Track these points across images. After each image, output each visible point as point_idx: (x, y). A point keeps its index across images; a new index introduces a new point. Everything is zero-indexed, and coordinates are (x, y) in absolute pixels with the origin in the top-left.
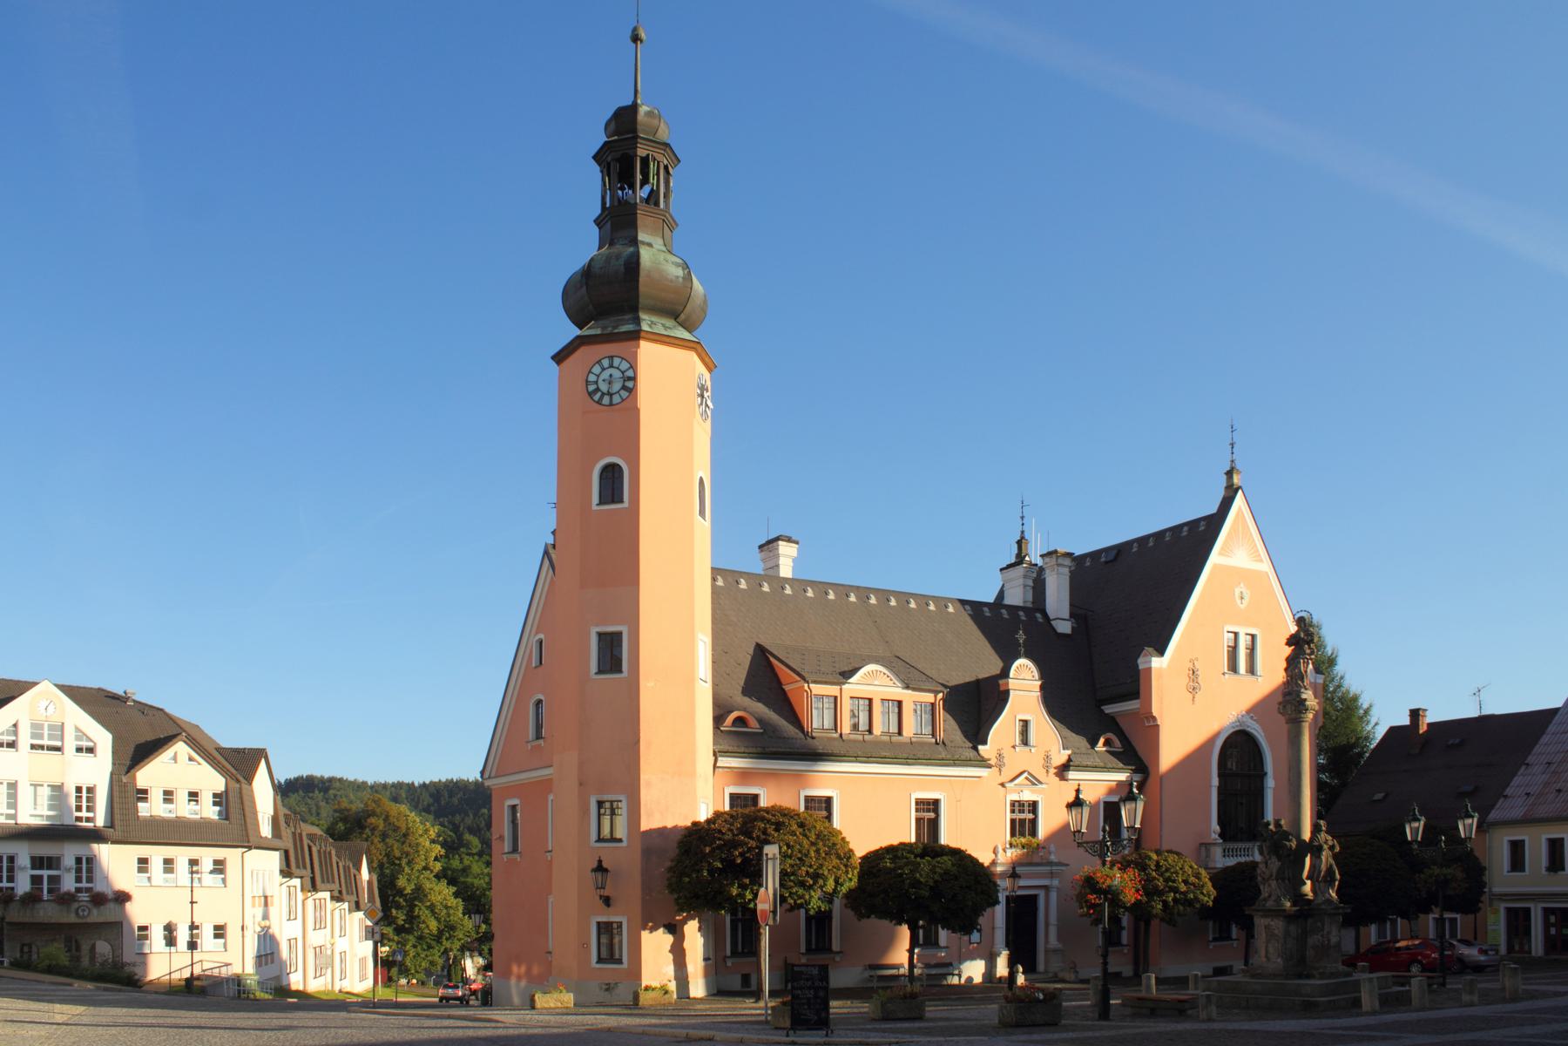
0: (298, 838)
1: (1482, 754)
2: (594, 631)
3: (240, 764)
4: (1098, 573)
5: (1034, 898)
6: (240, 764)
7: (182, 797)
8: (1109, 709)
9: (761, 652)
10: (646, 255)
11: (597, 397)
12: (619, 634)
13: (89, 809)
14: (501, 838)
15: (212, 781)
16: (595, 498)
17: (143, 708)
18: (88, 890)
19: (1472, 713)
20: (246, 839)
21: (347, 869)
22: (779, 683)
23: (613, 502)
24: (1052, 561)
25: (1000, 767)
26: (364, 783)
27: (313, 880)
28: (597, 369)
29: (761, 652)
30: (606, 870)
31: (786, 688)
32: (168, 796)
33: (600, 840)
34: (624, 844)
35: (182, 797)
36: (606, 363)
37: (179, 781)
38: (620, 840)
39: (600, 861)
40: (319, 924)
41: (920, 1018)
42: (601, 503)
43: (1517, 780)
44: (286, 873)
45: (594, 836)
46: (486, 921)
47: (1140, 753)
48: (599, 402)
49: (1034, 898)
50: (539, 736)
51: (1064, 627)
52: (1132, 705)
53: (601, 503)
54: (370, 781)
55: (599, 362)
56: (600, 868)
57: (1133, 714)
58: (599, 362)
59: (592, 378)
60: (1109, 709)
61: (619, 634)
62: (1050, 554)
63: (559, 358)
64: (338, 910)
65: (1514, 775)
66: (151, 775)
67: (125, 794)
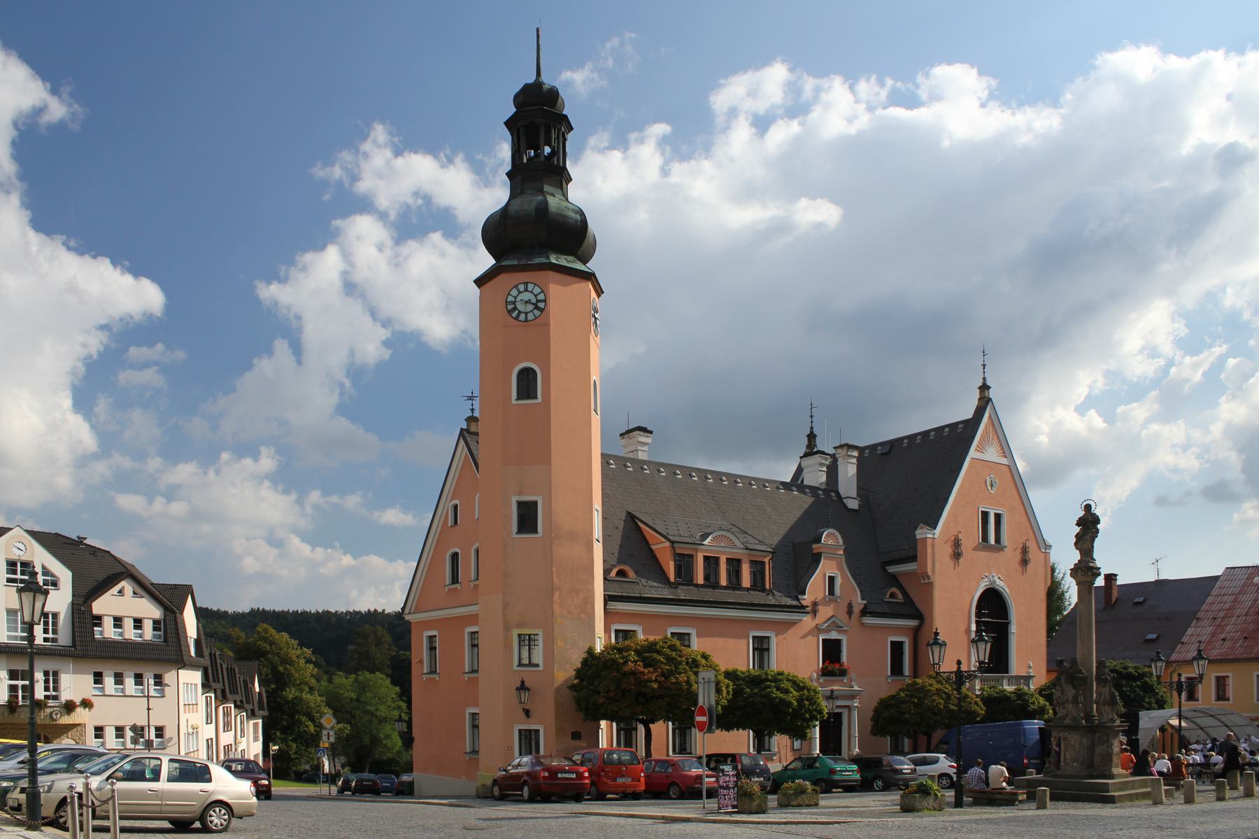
0: (213, 657)
1: (1164, 608)
2: (514, 499)
3: (170, 598)
4: (880, 460)
5: (840, 714)
6: (170, 598)
7: (128, 624)
8: (892, 569)
9: (631, 518)
10: (550, 199)
11: (514, 314)
12: (535, 503)
13: (55, 632)
14: (421, 662)
15: (150, 611)
16: (514, 395)
17: (95, 551)
18: (55, 698)
19: (1151, 578)
20: (181, 662)
21: (245, 682)
22: (648, 544)
23: (528, 397)
24: (839, 451)
25: (814, 612)
26: (226, 613)
27: (223, 692)
28: (514, 292)
29: (631, 518)
30: (528, 689)
31: (653, 547)
32: (118, 622)
33: (520, 665)
34: (541, 668)
35: (128, 624)
36: (522, 287)
37: (123, 611)
38: (537, 665)
39: (523, 682)
40: (227, 726)
41: (816, 805)
42: (518, 399)
43: (1190, 631)
44: (206, 686)
45: (516, 662)
46: (982, 721)
47: (917, 604)
48: (516, 318)
49: (840, 714)
50: (455, 579)
51: (853, 504)
52: (910, 567)
53: (518, 399)
54: (230, 611)
55: (516, 287)
56: (522, 687)
57: (913, 574)
58: (516, 287)
59: (510, 299)
60: (892, 569)
61: (535, 503)
62: (841, 446)
63: (480, 282)
64: (237, 717)
65: (1188, 626)
66: (104, 605)
67: (83, 617)
